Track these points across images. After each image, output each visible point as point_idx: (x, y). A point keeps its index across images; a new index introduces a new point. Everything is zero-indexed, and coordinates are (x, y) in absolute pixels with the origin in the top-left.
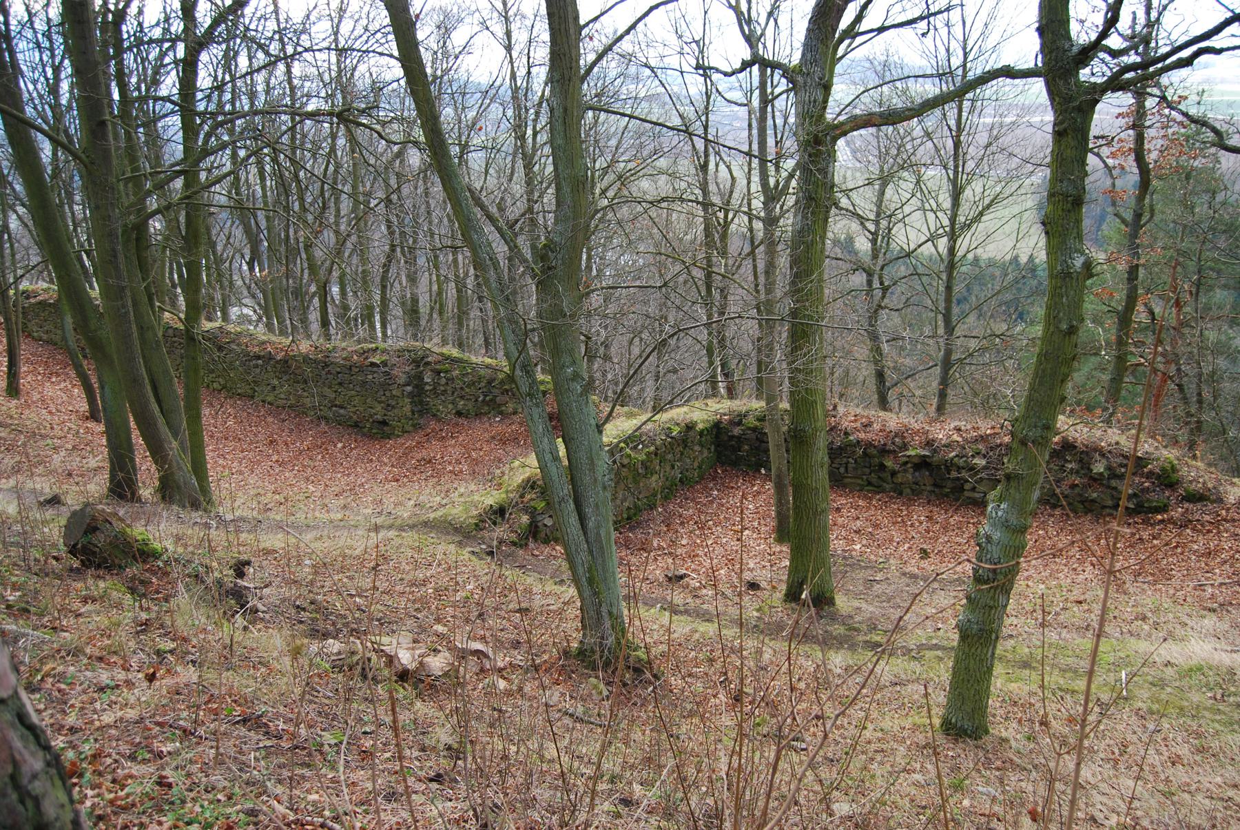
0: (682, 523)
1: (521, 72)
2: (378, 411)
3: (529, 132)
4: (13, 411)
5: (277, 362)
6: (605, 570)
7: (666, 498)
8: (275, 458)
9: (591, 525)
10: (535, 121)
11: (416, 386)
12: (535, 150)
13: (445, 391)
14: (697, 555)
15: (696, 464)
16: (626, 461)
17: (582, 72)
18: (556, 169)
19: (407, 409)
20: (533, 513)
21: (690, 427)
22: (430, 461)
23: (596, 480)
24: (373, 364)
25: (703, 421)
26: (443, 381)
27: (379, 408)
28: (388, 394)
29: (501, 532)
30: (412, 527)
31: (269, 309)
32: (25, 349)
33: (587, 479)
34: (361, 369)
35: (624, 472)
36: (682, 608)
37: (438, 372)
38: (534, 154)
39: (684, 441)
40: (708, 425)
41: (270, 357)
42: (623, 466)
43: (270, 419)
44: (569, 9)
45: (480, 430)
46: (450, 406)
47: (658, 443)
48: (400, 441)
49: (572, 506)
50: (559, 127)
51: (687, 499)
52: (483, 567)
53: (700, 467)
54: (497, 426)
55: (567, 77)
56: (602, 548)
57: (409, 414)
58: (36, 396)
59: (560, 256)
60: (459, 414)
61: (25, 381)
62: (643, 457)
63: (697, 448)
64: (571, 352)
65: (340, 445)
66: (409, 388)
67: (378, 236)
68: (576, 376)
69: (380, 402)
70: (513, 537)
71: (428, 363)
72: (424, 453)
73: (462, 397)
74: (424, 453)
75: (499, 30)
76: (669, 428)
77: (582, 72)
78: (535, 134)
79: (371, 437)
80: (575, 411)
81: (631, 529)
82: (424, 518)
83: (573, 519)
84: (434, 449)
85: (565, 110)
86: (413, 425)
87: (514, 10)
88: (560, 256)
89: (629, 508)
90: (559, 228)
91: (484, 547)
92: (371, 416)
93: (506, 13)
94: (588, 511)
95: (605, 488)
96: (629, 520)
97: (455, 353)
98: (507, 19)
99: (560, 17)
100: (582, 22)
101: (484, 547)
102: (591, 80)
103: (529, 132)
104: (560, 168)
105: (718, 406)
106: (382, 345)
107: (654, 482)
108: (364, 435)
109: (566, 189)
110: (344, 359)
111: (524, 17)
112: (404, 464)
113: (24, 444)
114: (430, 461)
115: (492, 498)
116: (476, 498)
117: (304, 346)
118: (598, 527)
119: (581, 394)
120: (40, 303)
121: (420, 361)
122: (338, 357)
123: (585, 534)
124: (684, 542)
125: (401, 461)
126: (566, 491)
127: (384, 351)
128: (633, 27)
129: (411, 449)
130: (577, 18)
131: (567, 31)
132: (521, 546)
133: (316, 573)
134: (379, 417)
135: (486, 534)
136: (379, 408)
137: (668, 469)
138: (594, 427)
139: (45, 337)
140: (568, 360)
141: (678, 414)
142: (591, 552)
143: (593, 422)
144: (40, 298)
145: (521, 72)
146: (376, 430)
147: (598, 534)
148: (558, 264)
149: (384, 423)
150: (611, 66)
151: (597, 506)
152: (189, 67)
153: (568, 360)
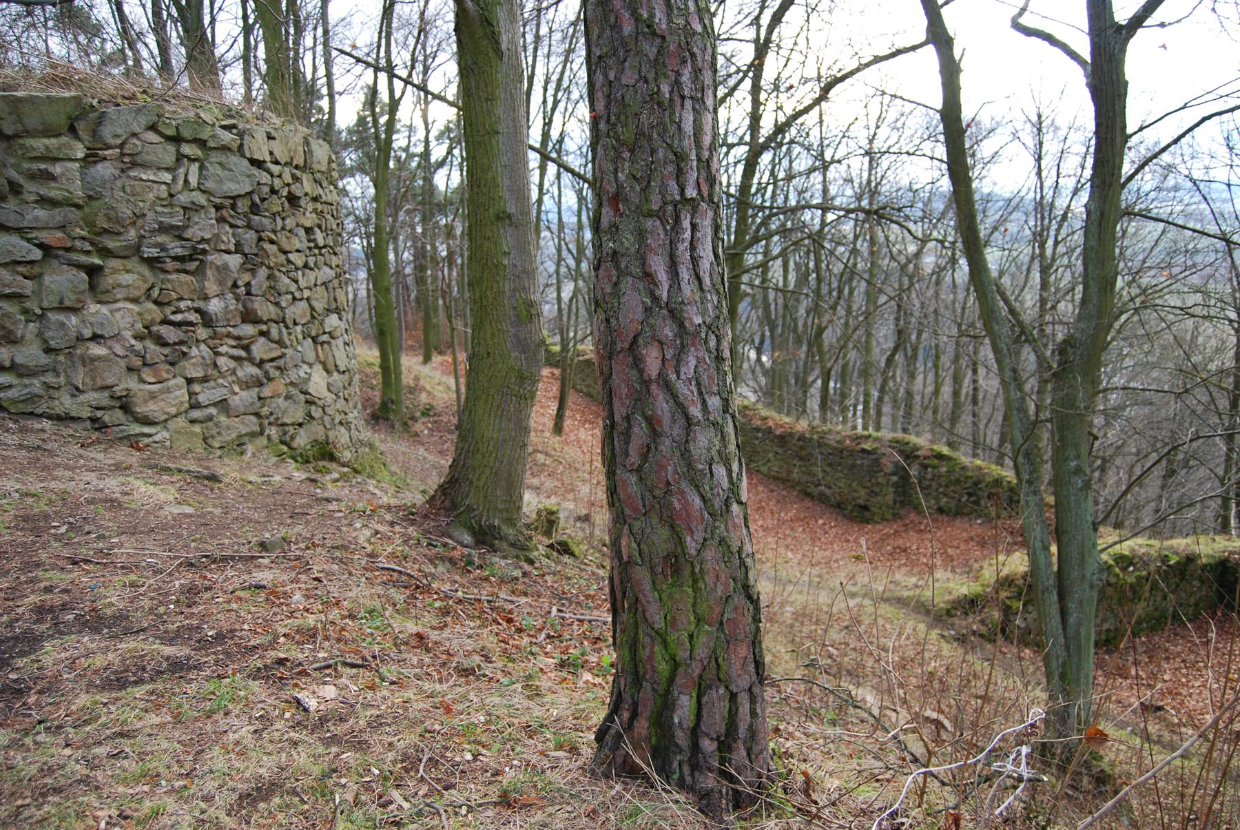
0: (1167, 659)
1: (1049, 183)
2: (862, 495)
3: (1050, 242)
4: (557, 446)
5: (776, 436)
6: (1079, 668)
7: (1152, 629)
8: (760, 523)
9: (1071, 620)
10: (1058, 230)
11: (902, 477)
12: (1053, 259)
13: (930, 486)
14: (1180, 694)
15: (1192, 601)
16: (1113, 580)
17: (1123, 180)
18: (1086, 269)
19: (890, 498)
20: (1007, 611)
21: (1190, 559)
22: (905, 550)
23: (1083, 577)
24: (863, 450)
25: (1207, 556)
26: (929, 476)
27: (863, 492)
28: (873, 480)
29: (973, 623)
30: (886, 600)
31: (771, 394)
32: (572, 398)
33: (1075, 574)
34: (852, 453)
35: (1110, 591)
36: (1156, 738)
37: (926, 467)
38: (1051, 266)
39: (1181, 573)
40: (1212, 561)
41: (769, 431)
42: (1109, 584)
43: (760, 488)
44: (1118, 119)
45: (960, 529)
46: (933, 502)
47: (1152, 567)
48: (878, 526)
49: (1056, 597)
50: (1094, 229)
51: (1176, 635)
52: (949, 650)
53: (1196, 605)
54: (977, 527)
55: (1107, 183)
56: (1079, 647)
57: (891, 503)
58: (573, 437)
59: (1078, 352)
60: (941, 510)
61: (567, 423)
62: (1131, 579)
63: (1196, 583)
64: (1077, 446)
65: (821, 522)
66: (895, 478)
67: (884, 335)
68: (1078, 471)
69: (865, 488)
70: (984, 630)
71: (917, 457)
72: (900, 542)
73: (945, 495)
74: (900, 542)
75: (1029, 139)
76: (1166, 556)
77: (1123, 180)
78: (1056, 243)
79: (851, 519)
80: (1073, 505)
81: (1108, 652)
82: (898, 594)
83: (1054, 610)
84: (911, 540)
85: (1102, 213)
86: (894, 515)
87: (1049, 121)
88: (1078, 352)
89: (1108, 631)
90: (1082, 325)
91: (953, 632)
92: (854, 499)
93: (1040, 123)
94: (1072, 606)
95: (1092, 587)
96: (1107, 643)
97: (945, 450)
98: (1039, 130)
99: (1107, 127)
100: (1129, 131)
101: (953, 632)
102: (1133, 185)
103: (1050, 242)
104: (1090, 268)
105: (1227, 544)
106: (875, 434)
107: (1140, 609)
108: (845, 516)
109: (1094, 289)
110: (838, 442)
111: (1057, 128)
112: (880, 548)
113: (561, 473)
114: (905, 550)
115: (963, 587)
116: (951, 585)
117: (802, 425)
118: (1079, 624)
119: (1082, 489)
120: (586, 361)
121: (910, 454)
122: (831, 440)
123: (1064, 628)
124: (1166, 677)
125: (876, 546)
126: (1051, 582)
127: (877, 439)
128: (1176, 141)
129: (888, 536)
130: (1124, 127)
131: (1113, 140)
132: (990, 641)
133: (796, 620)
134: (861, 502)
135: (956, 620)
136: (863, 492)
137: (1159, 599)
138: (1089, 524)
139: (585, 390)
140: (1072, 454)
141: (1181, 544)
142: (1067, 648)
143: (1090, 519)
144: (587, 357)
145: (1049, 183)
146: (858, 514)
147: (1078, 632)
148: (1077, 361)
149: (865, 508)
150: (1147, 181)
151: (1081, 603)
152: (751, 165)
153: (1072, 454)
